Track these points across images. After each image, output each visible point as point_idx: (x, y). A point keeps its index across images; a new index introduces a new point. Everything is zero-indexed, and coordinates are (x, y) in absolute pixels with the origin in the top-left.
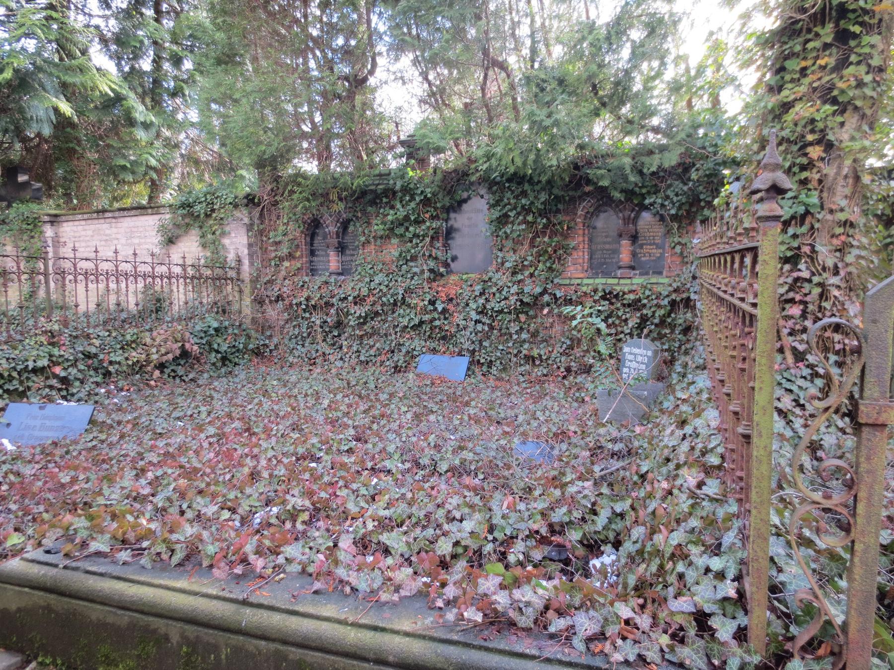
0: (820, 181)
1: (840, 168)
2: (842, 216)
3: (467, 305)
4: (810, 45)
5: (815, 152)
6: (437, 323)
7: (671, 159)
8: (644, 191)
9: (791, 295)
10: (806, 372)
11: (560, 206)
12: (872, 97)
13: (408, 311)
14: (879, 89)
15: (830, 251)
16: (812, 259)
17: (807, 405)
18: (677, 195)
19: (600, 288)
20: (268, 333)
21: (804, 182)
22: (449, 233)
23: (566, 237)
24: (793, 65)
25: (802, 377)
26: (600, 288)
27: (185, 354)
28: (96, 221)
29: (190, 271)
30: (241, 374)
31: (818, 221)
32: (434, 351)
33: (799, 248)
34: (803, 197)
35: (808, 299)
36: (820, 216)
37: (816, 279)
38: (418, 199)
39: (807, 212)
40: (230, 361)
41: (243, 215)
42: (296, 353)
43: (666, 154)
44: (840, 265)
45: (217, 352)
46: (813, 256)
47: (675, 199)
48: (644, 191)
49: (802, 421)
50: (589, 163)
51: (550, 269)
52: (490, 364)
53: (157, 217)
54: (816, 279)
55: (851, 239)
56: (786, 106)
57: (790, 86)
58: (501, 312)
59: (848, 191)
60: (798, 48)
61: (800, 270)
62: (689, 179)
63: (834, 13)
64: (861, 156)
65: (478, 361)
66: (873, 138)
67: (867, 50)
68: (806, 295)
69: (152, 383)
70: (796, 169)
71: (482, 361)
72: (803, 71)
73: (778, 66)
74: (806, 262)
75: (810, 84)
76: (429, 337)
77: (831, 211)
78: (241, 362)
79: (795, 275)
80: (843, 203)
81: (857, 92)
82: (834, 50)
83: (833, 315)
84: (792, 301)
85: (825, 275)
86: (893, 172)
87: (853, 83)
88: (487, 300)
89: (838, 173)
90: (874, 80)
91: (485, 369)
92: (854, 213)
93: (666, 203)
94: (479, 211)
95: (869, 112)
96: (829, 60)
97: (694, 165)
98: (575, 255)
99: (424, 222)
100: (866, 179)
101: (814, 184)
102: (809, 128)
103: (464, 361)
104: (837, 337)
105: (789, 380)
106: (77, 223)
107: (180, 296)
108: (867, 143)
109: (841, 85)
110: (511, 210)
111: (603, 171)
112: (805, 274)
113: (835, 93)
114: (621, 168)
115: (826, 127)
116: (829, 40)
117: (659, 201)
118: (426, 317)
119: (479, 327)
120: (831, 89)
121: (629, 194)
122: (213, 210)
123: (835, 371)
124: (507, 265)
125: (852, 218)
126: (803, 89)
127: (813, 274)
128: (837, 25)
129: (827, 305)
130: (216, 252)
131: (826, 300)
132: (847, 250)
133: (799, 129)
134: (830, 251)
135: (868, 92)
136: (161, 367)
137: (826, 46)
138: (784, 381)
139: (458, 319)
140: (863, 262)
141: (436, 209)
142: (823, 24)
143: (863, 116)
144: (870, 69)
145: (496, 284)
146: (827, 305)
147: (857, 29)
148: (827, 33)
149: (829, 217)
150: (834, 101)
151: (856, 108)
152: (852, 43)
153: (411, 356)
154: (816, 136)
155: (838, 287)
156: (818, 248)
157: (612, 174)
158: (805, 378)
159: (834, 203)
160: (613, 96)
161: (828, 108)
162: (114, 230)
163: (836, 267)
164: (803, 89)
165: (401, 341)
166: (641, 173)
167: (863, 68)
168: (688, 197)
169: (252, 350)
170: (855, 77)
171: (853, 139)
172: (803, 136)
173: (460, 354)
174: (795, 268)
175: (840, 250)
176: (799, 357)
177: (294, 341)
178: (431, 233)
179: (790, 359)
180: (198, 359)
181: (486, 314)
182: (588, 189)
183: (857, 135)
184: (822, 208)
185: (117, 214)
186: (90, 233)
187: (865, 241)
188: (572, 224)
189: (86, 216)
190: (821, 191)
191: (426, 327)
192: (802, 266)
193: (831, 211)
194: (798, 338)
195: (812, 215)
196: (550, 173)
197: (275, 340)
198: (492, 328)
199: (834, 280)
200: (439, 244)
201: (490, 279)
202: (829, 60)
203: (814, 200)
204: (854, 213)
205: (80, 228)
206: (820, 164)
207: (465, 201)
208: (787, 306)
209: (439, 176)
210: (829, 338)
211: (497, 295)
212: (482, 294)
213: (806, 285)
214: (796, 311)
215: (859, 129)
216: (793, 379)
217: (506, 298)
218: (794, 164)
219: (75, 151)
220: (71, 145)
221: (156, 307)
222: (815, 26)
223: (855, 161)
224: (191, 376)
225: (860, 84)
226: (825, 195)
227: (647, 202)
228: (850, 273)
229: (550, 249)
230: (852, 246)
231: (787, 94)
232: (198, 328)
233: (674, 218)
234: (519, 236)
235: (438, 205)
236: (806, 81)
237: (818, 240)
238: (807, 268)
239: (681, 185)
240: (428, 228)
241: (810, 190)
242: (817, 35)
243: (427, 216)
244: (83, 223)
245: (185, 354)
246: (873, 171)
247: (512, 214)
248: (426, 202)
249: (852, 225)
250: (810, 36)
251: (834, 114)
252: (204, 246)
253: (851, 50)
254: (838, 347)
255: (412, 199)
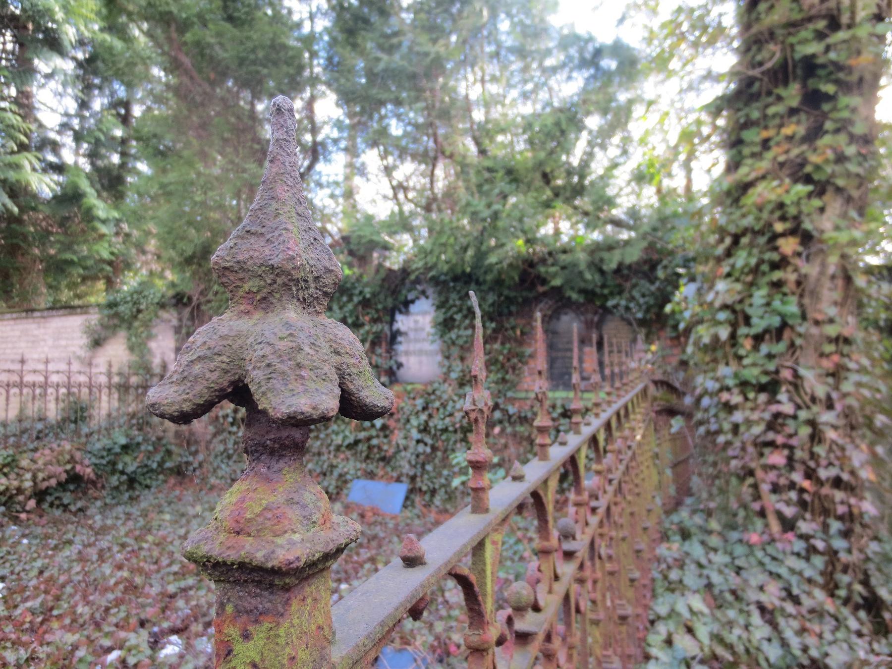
0: (799, 283)
1: (824, 265)
2: (831, 330)
3: (408, 421)
4: (771, 110)
5: (788, 245)
6: (375, 442)
7: (633, 256)
8: (606, 291)
9: (771, 436)
10: (799, 546)
11: (513, 309)
12: (858, 175)
13: (343, 427)
14: (866, 165)
15: (820, 376)
16: (796, 386)
17: (804, 599)
18: (643, 296)
19: (559, 403)
20: (193, 449)
21: (777, 285)
22: (395, 336)
23: (521, 342)
24: (753, 136)
25: (793, 553)
26: (559, 403)
27: (74, 478)
28: (25, 321)
29: (116, 379)
30: (147, 499)
31: (800, 335)
32: (371, 475)
33: (777, 372)
34: (777, 304)
35: (794, 442)
36: (801, 329)
37: (803, 415)
38: (356, 299)
39: (784, 325)
40: (140, 484)
41: (171, 316)
42: (220, 473)
43: (629, 249)
44: (835, 395)
45: (122, 473)
46: (797, 383)
47: (642, 301)
48: (606, 291)
49: (796, 624)
50: (543, 261)
51: (504, 380)
52: (433, 492)
53: (84, 317)
54: (803, 415)
55: (846, 361)
56: (745, 187)
57: (749, 161)
58: (445, 430)
59: (837, 295)
60: (755, 115)
61: (779, 402)
62: (657, 278)
63: (799, 72)
64: (850, 251)
65: (420, 490)
66: (865, 227)
67: (845, 114)
68: (790, 436)
69: (23, 516)
70: (765, 267)
71: (424, 488)
72: (766, 144)
73: (733, 138)
74: (788, 391)
75: (775, 158)
76: (367, 457)
77: (817, 323)
78: (154, 483)
79: (774, 408)
80: (832, 311)
81: (838, 169)
82: (803, 116)
83: (830, 464)
84: (772, 444)
85: (815, 409)
86: (891, 271)
87: (830, 155)
88: (430, 416)
89: (822, 273)
90: (859, 154)
91: (427, 497)
92: (849, 325)
93: (632, 305)
94: (424, 313)
95: (855, 194)
96: (796, 128)
97: (661, 260)
98: (532, 364)
99: (362, 325)
100: (860, 281)
101: (790, 287)
102: (778, 214)
103: (402, 489)
104: (839, 495)
105: (774, 559)
106: (5, 323)
107: (105, 405)
108: (857, 234)
109: (814, 158)
110: (457, 313)
111: (553, 269)
112: (787, 408)
113: (808, 169)
114: (575, 265)
115: (800, 212)
116: (795, 103)
117: (623, 303)
118: (362, 435)
119: (421, 448)
120: (802, 165)
121: (590, 295)
122: (139, 311)
123: (839, 544)
124: (454, 375)
125: (846, 332)
126: (764, 165)
127: (798, 407)
128: (804, 85)
129: (820, 450)
130: (142, 356)
131: (820, 441)
132: (843, 374)
133: (765, 215)
134: (820, 376)
135: (853, 168)
136: (40, 495)
137: (793, 112)
138: (767, 560)
139: (398, 437)
140: (866, 393)
141: (377, 311)
142: (786, 83)
143: (849, 200)
144: (852, 138)
145: (440, 398)
146: (820, 450)
147: (830, 89)
148: (792, 94)
149: (814, 331)
150: (808, 179)
151: (839, 190)
152: (826, 107)
153: (343, 481)
154: (788, 225)
155: (835, 427)
156: (802, 371)
157: (566, 272)
158: (798, 555)
159: (820, 311)
160: (572, 190)
161: (801, 189)
162: (42, 331)
163: (829, 398)
164: (764, 165)
165: (335, 462)
166: (602, 272)
167: (842, 138)
168: (656, 298)
169: (171, 469)
170: (834, 150)
171: (837, 228)
172: (770, 225)
173: (398, 480)
174: (773, 400)
175: (833, 375)
176: (788, 525)
177: (219, 459)
178: (371, 337)
179: (775, 527)
180: (94, 483)
181: (429, 433)
182: (541, 289)
183: (843, 223)
184: (804, 317)
185: (46, 313)
186: (17, 333)
187: (865, 362)
188: (526, 330)
189: (14, 315)
190: (801, 296)
191: (362, 447)
192: (783, 396)
193: (817, 323)
194: (784, 497)
195: (792, 328)
196: (495, 272)
197: (201, 457)
198: (434, 449)
199: (827, 417)
200: (379, 351)
201: (434, 392)
202: (796, 128)
203: (792, 308)
204: (849, 325)
205: (8, 328)
206: (797, 261)
207: (413, 302)
208: (767, 451)
209: (382, 274)
210: (826, 496)
211: (441, 410)
212: (425, 409)
213: (790, 422)
214: (778, 458)
215: (844, 216)
216: (780, 556)
217: (451, 415)
218: (761, 262)
219: (19, 247)
220: (15, 241)
221: (77, 414)
222: (776, 86)
223: (844, 256)
224: (79, 504)
225: (841, 158)
226: (806, 301)
227: (610, 303)
228: (850, 407)
229: (501, 358)
230: (848, 370)
231: (744, 172)
232: (98, 446)
233: (642, 323)
234: (466, 342)
235: (380, 306)
236: (769, 155)
237: (802, 361)
238: (791, 399)
239: (647, 285)
240: (368, 332)
241: (785, 294)
242: (779, 98)
243: (367, 318)
244: (12, 322)
245: (74, 478)
246: (869, 270)
247: (458, 317)
248: (366, 303)
249: (847, 341)
250: (770, 99)
251: (810, 195)
252: (131, 349)
253: (825, 116)
254: (841, 509)
255: (350, 300)
